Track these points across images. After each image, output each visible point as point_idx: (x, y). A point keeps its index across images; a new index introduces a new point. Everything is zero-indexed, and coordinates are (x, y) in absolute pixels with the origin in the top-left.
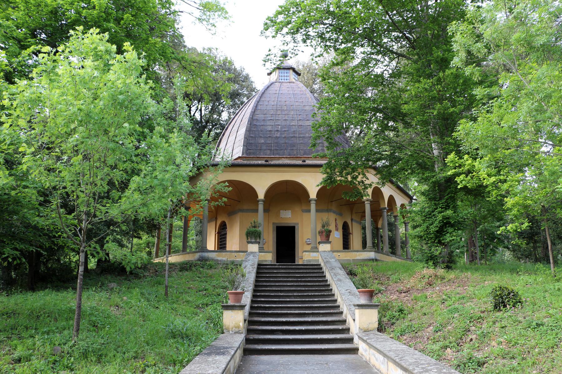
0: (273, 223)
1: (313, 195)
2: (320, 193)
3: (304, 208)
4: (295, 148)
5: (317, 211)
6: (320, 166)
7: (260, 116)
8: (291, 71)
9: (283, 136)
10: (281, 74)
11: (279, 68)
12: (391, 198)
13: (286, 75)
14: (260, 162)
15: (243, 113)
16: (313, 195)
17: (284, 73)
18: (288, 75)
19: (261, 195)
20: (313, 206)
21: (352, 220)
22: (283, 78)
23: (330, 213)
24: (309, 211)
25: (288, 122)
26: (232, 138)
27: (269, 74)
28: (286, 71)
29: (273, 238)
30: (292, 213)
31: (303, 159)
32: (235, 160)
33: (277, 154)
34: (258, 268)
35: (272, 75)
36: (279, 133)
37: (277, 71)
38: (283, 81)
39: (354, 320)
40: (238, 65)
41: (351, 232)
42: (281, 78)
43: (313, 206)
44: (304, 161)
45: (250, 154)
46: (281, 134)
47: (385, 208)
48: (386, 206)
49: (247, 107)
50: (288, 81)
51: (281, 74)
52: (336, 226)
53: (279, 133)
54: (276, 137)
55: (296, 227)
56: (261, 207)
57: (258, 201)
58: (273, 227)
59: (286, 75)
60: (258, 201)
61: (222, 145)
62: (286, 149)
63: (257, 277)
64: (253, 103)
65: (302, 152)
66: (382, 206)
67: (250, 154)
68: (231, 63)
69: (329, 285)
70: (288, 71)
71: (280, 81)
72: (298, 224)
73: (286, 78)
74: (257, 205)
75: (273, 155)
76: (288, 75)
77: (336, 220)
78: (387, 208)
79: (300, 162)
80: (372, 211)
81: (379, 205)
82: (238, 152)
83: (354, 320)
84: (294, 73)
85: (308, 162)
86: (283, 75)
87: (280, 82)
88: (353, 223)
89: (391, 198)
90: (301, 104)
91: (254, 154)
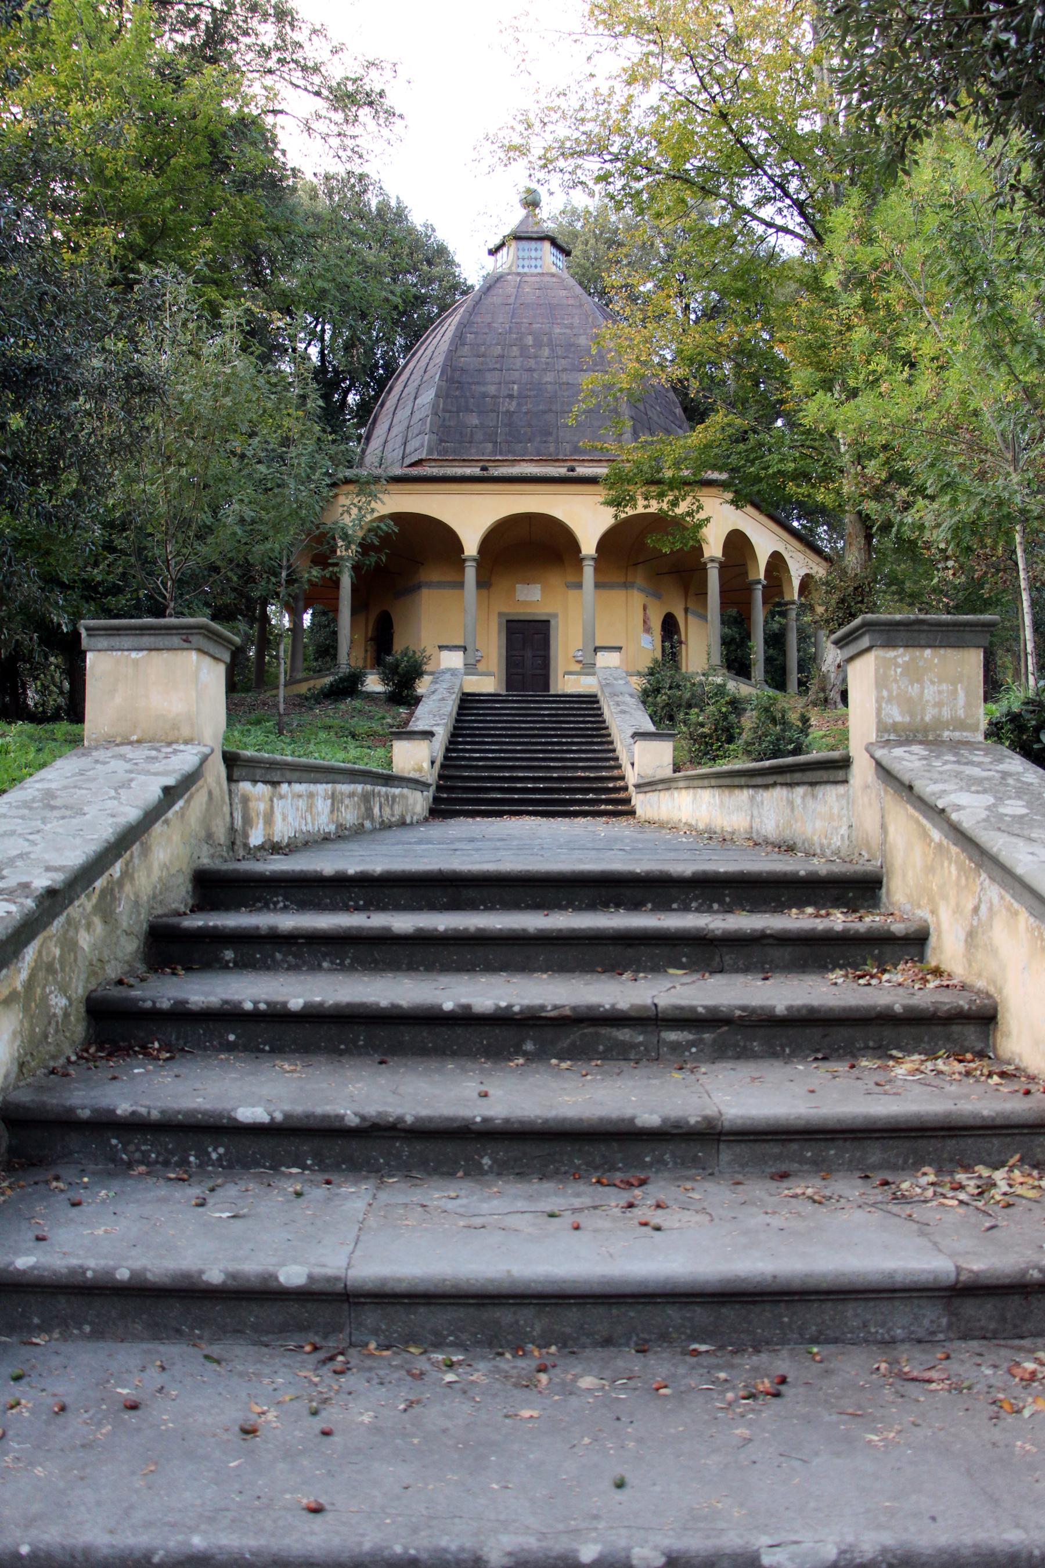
0: (500, 614)
1: (588, 546)
2: (608, 542)
3: (571, 578)
4: (551, 439)
5: (598, 585)
6: (592, 481)
7: (467, 359)
8: (547, 245)
9: (524, 409)
10: (521, 254)
11: (517, 237)
12: (777, 561)
13: (533, 254)
14: (468, 471)
15: (429, 352)
16: (588, 546)
17: (530, 250)
18: (539, 254)
19: (471, 547)
20: (589, 571)
21: (686, 610)
22: (526, 263)
23: (630, 591)
24: (579, 586)
25: (535, 375)
26: (403, 414)
27: (493, 252)
28: (533, 244)
29: (499, 648)
30: (543, 590)
31: (569, 464)
32: (412, 465)
33: (509, 452)
34: (462, 700)
35: (499, 255)
36: (514, 403)
37: (514, 243)
38: (526, 270)
39: (633, 764)
40: (417, 219)
41: (683, 638)
42: (521, 263)
43: (589, 571)
44: (573, 470)
45: (446, 452)
46: (519, 405)
47: (758, 582)
48: (762, 576)
49: (439, 337)
50: (539, 270)
51: (521, 254)
52: (645, 622)
53: (514, 403)
54: (508, 411)
55: (553, 623)
56: (470, 573)
57: (464, 560)
58: (500, 624)
59: (533, 254)
60: (464, 560)
61: (380, 430)
62: (530, 440)
63: (460, 708)
64: (453, 328)
65: (568, 446)
66: (752, 577)
67: (446, 452)
68: (400, 215)
69: (607, 728)
70: (538, 245)
71: (520, 270)
72: (556, 616)
73: (533, 263)
74: (462, 570)
75: (501, 454)
76: (539, 254)
77: (645, 608)
78: (765, 582)
79: (561, 471)
80: (723, 592)
81: (746, 574)
82: (420, 446)
83: (633, 764)
84: (554, 251)
85: (582, 471)
86: (526, 254)
87: (519, 274)
88: (690, 617)
89: (777, 561)
90: (568, 331)
91: (455, 453)
